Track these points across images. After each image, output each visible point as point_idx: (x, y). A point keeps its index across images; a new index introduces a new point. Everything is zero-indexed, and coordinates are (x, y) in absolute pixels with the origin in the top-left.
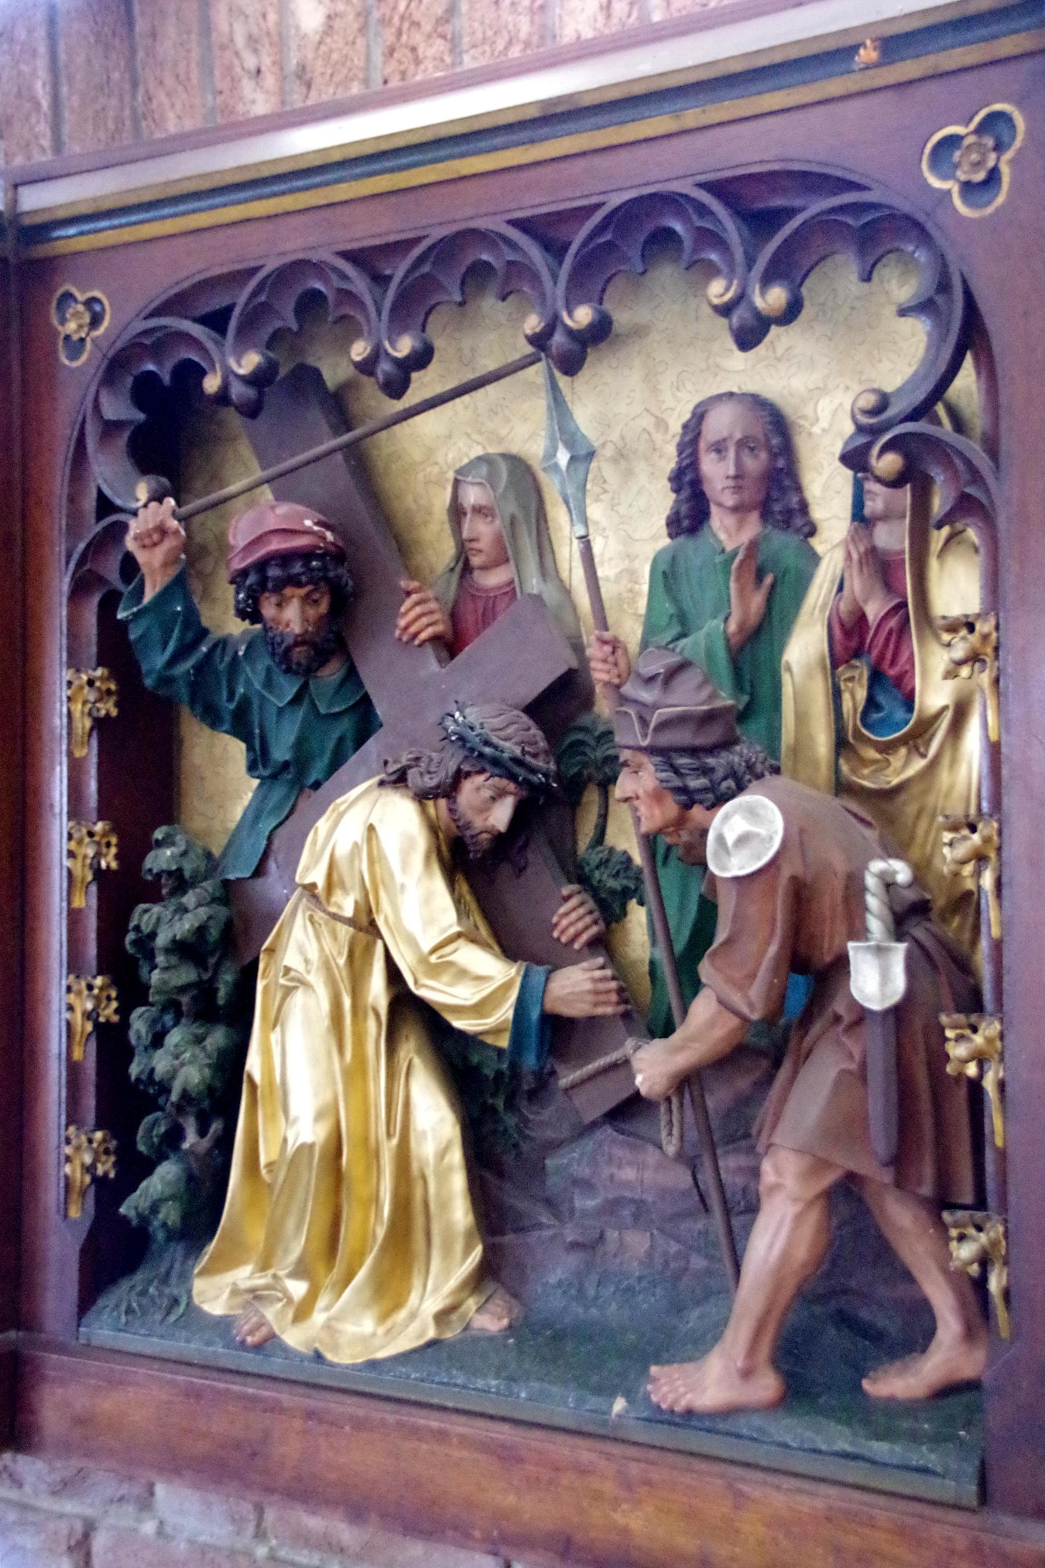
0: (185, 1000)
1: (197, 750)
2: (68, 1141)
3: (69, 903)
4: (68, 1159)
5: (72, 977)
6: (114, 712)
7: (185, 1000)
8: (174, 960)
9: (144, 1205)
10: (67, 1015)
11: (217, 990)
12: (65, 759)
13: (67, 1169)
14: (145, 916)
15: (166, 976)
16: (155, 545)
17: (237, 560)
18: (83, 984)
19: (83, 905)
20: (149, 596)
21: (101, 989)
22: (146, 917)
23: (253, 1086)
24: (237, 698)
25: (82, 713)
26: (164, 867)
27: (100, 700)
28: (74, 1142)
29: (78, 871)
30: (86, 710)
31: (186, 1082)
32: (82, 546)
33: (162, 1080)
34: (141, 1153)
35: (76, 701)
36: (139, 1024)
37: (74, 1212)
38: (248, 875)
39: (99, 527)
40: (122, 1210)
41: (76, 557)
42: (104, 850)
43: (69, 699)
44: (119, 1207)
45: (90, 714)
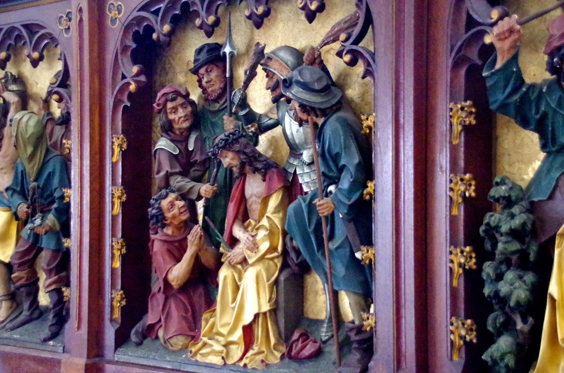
0: (514, 258)
1: (506, 142)
2: (452, 324)
3: (451, 211)
4: (452, 332)
5: (452, 247)
6: (474, 122)
7: (514, 258)
8: (510, 239)
9: (497, 355)
10: (451, 265)
11: (529, 254)
12: (448, 145)
13: (452, 337)
14: (492, 218)
15: (506, 246)
16: (506, 38)
17: (556, 42)
18: (459, 250)
19: (457, 213)
20: (498, 66)
21: (468, 253)
22: (493, 218)
23: (553, 300)
24: (541, 112)
25: (457, 123)
26: (502, 194)
27: (466, 117)
28: (455, 324)
29: (455, 198)
30: (459, 122)
31: (518, 296)
32: (459, 44)
33: (505, 296)
34: (489, 331)
35: (454, 118)
36: (488, 269)
37: (456, 358)
38: (545, 198)
39: (465, 36)
40: (483, 357)
41: (456, 49)
42: (468, 188)
43: (451, 117)
44: (482, 355)
45: (460, 124)
